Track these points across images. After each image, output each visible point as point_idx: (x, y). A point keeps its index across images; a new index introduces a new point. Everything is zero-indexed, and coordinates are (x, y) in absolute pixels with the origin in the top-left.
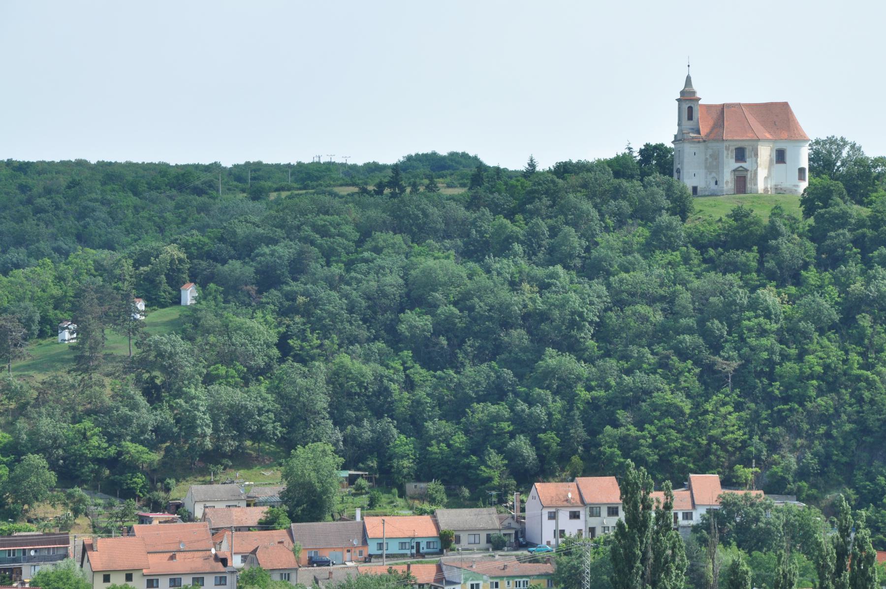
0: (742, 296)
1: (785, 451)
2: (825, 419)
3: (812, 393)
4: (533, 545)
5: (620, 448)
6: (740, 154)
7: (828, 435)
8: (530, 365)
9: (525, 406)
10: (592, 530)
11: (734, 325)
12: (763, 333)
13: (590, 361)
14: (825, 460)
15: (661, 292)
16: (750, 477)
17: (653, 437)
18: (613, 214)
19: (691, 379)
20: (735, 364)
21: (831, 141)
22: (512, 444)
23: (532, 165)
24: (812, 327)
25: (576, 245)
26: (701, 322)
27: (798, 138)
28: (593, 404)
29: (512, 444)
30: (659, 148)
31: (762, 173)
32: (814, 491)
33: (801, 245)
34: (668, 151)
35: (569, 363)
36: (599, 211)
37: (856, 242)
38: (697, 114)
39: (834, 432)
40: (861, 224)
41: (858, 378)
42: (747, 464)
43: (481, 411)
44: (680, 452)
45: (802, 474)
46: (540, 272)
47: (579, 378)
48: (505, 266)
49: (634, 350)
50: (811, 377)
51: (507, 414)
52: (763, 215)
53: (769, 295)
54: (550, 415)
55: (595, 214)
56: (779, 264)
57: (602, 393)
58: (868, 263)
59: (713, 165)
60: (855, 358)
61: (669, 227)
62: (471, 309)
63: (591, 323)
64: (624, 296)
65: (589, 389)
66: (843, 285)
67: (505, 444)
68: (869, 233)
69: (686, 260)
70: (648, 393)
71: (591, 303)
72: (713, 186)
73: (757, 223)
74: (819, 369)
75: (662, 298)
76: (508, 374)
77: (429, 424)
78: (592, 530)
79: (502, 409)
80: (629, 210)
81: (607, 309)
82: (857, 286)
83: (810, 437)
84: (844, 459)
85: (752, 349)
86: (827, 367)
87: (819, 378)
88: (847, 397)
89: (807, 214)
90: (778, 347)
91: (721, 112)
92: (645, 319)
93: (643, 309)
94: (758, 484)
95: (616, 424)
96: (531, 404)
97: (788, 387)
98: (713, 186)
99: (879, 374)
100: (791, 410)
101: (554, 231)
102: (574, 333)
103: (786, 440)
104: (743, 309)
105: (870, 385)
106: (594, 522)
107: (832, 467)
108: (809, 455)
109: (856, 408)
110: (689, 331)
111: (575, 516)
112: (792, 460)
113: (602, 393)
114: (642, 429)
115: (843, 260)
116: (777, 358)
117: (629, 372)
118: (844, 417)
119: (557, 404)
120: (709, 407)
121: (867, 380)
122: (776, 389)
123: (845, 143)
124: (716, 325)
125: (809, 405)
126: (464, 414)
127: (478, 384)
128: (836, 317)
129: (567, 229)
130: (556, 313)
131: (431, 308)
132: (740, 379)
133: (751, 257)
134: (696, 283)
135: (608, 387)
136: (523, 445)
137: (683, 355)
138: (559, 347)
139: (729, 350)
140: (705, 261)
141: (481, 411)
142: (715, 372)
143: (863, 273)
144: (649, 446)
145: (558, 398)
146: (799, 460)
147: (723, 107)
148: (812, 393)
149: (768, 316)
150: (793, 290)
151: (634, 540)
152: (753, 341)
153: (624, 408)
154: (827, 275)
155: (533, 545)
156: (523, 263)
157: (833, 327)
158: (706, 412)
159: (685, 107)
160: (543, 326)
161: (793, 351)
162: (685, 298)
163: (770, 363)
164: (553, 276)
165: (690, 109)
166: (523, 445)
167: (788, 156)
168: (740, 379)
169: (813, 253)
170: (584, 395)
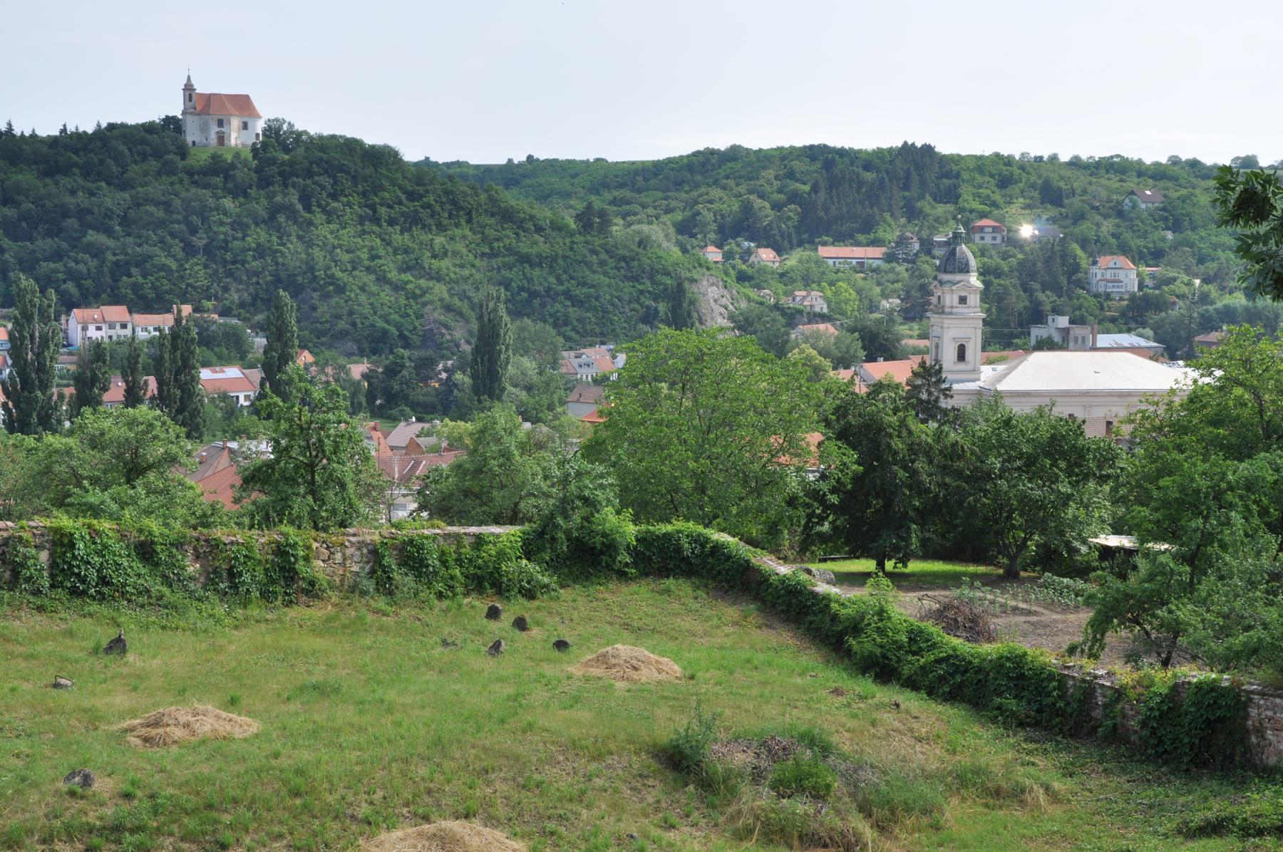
0: (211, 202)
1: (232, 292)
2: (257, 274)
3: (250, 259)
4: (71, 345)
5: (133, 290)
6: (221, 123)
7: (258, 283)
8: (78, 239)
9: (73, 264)
10: (110, 337)
11: (205, 219)
12: (222, 224)
13: (117, 239)
14: (255, 297)
15: (163, 198)
16: (211, 307)
17: (153, 284)
18: (139, 154)
19: (178, 250)
20: (204, 242)
21: (277, 120)
22: (63, 287)
23: (99, 125)
24: (251, 221)
25: (115, 170)
26: (186, 217)
27: (257, 116)
28: (117, 264)
29: (63, 287)
30: (174, 118)
31: (233, 136)
32: (248, 315)
33: (248, 175)
34: (180, 120)
35: (101, 238)
36: (131, 151)
37: (280, 174)
38: (194, 98)
39: (261, 281)
40: (283, 163)
41: (277, 251)
42: (209, 299)
43: (45, 267)
44: (169, 292)
45: (242, 305)
46: (90, 185)
47: (108, 248)
48: (66, 181)
49: (144, 233)
50: (249, 250)
51: (62, 269)
52: (229, 157)
53: (228, 203)
54: (89, 270)
55: (127, 153)
56: (235, 186)
57: (122, 257)
58: (286, 186)
59: (204, 128)
60: (274, 239)
61: (172, 162)
62: (43, 206)
63: (118, 216)
64: (141, 201)
65: (115, 255)
66: (270, 197)
67: (59, 286)
68: (288, 169)
69: (181, 181)
70: (151, 258)
71: (119, 204)
72: (204, 141)
73: (225, 161)
74: (254, 245)
75: (165, 203)
76: (65, 245)
77: (11, 274)
78: (110, 337)
79: (60, 266)
80: (150, 152)
81: (129, 208)
82: (278, 198)
83: (248, 284)
84: (266, 297)
85: (215, 233)
86: (258, 245)
87: (254, 250)
88: (269, 261)
89: (255, 157)
90: (230, 232)
91: (209, 99)
92: (151, 214)
93: (151, 208)
94: (215, 310)
95: (130, 276)
96: (77, 263)
97: (236, 255)
98: (204, 141)
99: (288, 249)
100: (237, 268)
101: (101, 162)
102: (107, 221)
103: (234, 286)
104: (211, 210)
105: (283, 254)
106: (111, 332)
107: (259, 301)
108: (246, 294)
109: (274, 267)
110: (178, 222)
111: (99, 328)
112: (236, 297)
113: (122, 257)
114: (145, 278)
115: (272, 184)
116: (230, 239)
117: (139, 245)
118: (267, 273)
119: (93, 264)
120: (187, 266)
121: (281, 252)
122: (229, 256)
123: (285, 121)
124: (194, 218)
125: (247, 266)
126: (35, 268)
127: (45, 250)
128: (266, 216)
129: (109, 161)
130: (96, 209)
131: (17, 204)
132: (208, 250)
133: (218, 180)
134: (184, 194)
135: (127, 254)
136: (70, 287)
137: (173, 235)
138: (97, 230)
139: (201, 233)
140: (193, 183)
141: (45, 267)
142: (193, 246)
143: (282, 192)
144: (150, 288)
145: (95, 260)
146: (240, 297)
147: (210, 95)
148: (250, 259)
149: (225, 214)
150: (242, 200)
151: (23, 326)
152: (215, 229)
153: (136, 267)
154: (262, 192)
155: (71, 345)
156: (80, 181)
157: (264, 221)
158: (186, 269)
159: (187, 93)
160: (88, 217)
161: (240, 235)
162: (177, 202)
163: (226, 241)
164: (99, 188)
165: (190, 95)
166: (70, 287)
167: (249, 126)
168: (208, 250)
169: (255, 179)
170: (110, 257)
